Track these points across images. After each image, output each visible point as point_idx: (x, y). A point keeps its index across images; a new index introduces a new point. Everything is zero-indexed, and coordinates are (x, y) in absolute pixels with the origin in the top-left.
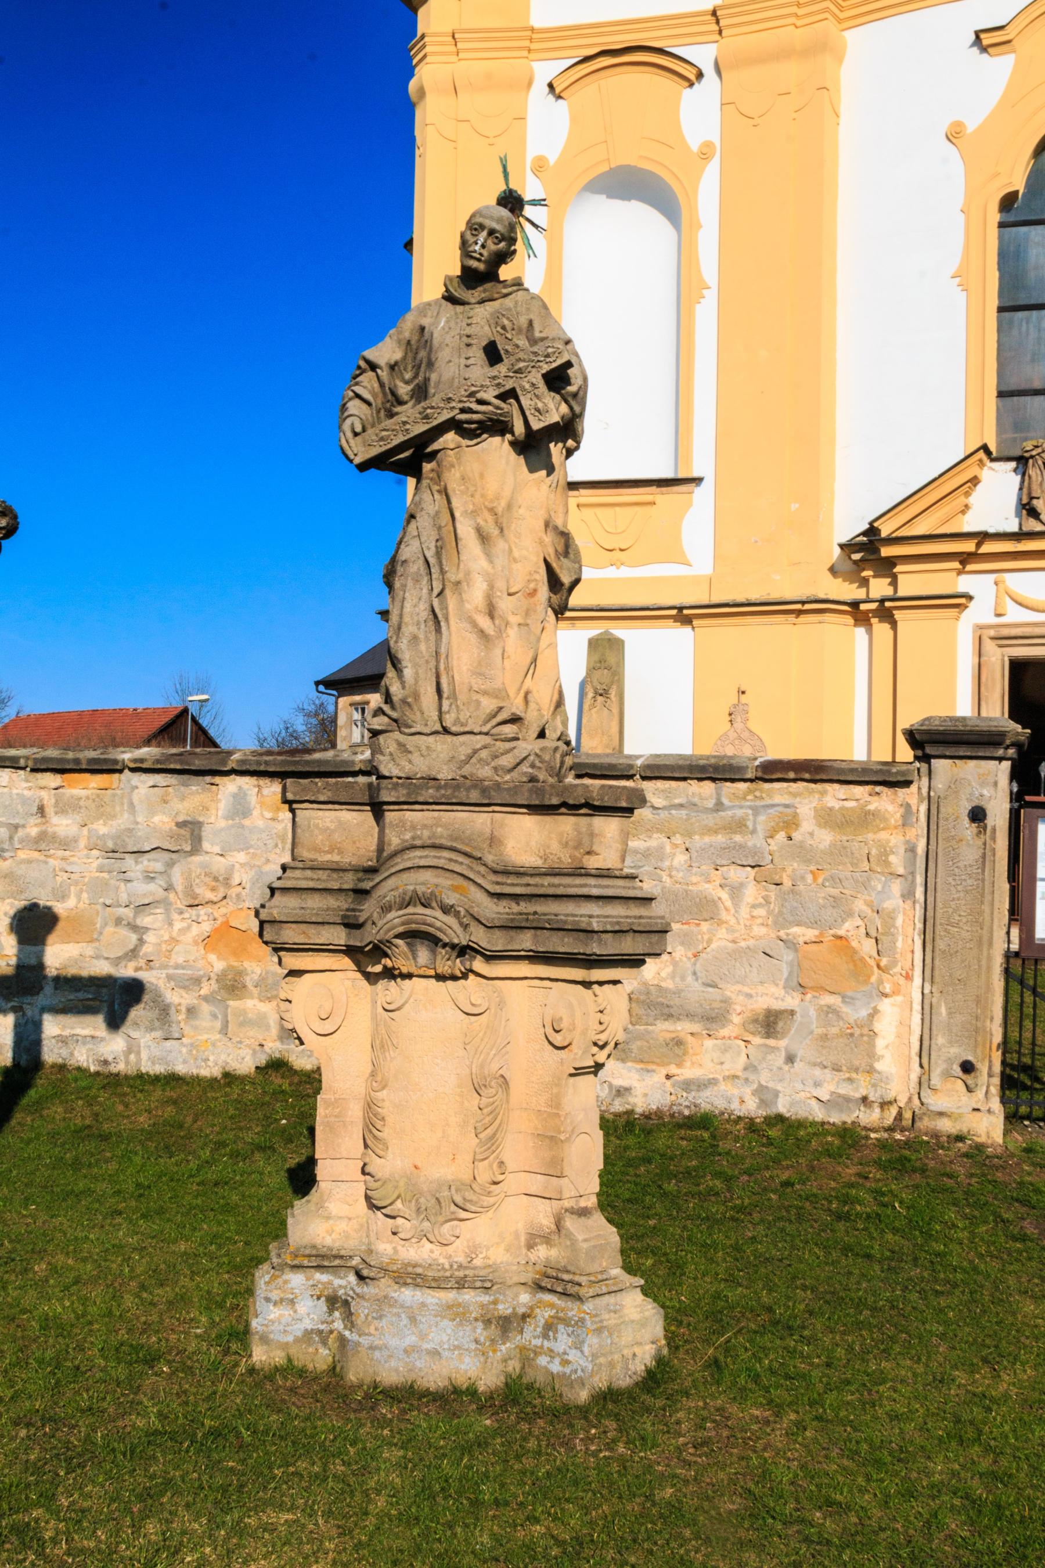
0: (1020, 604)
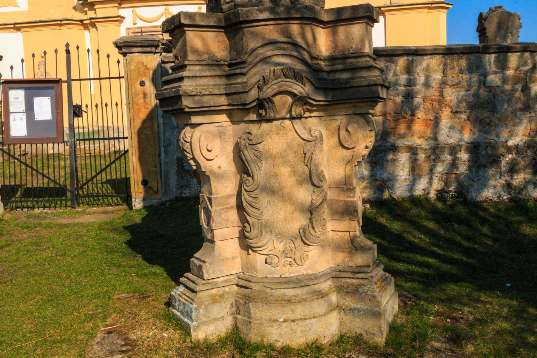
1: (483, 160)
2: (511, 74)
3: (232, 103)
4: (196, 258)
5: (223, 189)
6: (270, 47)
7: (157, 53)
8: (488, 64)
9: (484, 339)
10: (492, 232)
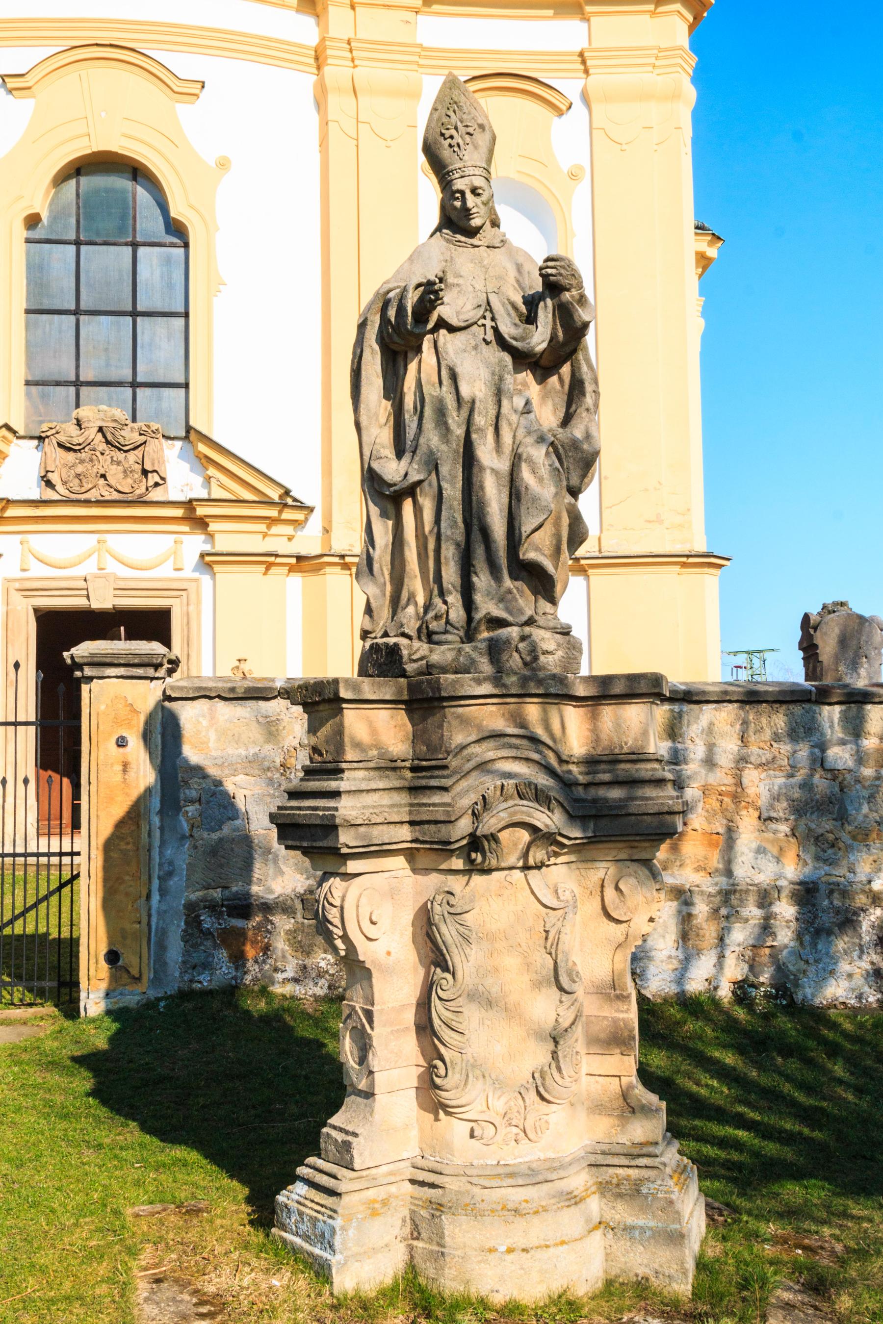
0: (41, 561)
1: (826, 919)
2: (873, 746)
3: (421, 838)
4: (334, 1127)
5: (394, 992)
6: (491, 744)
7: (157, 678)
8: (827, 725)
9: (868, 1286)
10: (852, 1074)
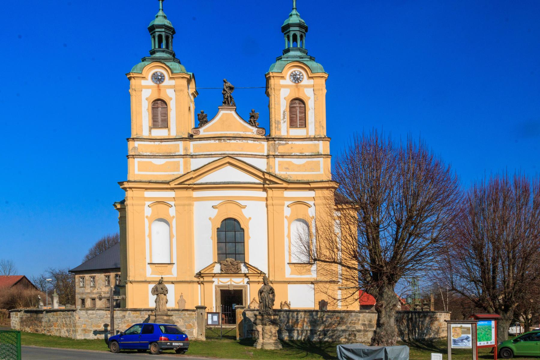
5: (261, 333)
